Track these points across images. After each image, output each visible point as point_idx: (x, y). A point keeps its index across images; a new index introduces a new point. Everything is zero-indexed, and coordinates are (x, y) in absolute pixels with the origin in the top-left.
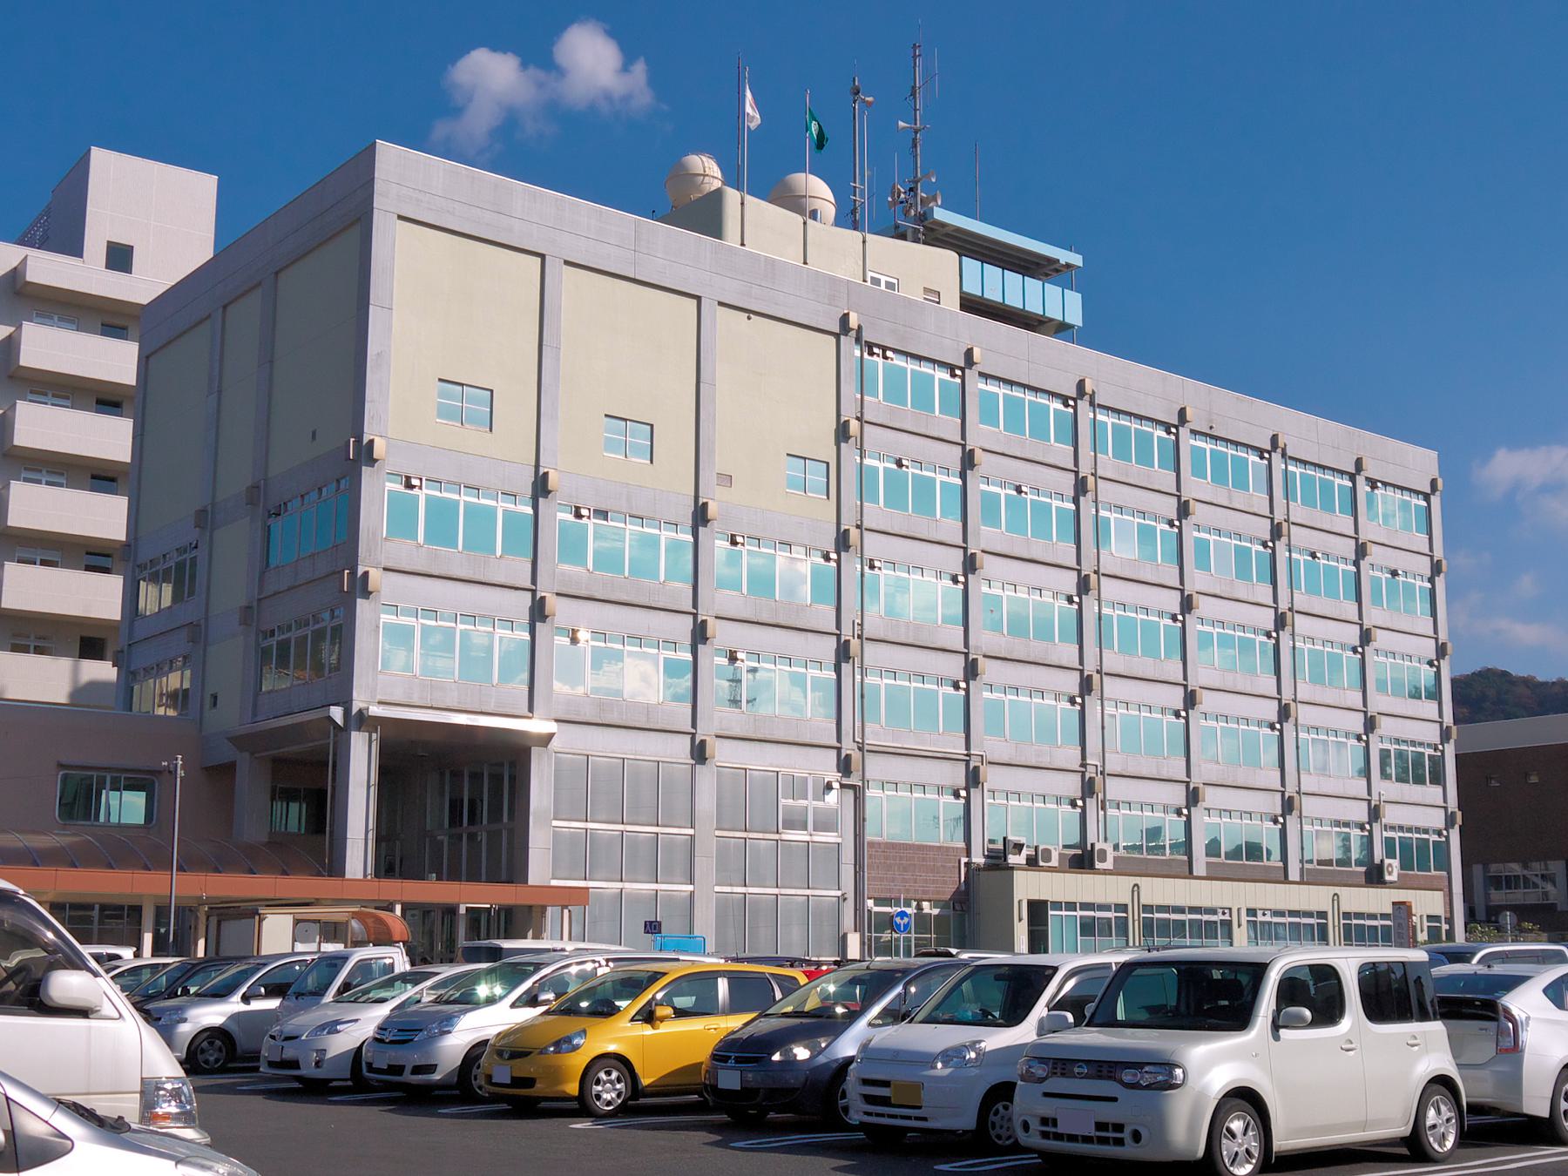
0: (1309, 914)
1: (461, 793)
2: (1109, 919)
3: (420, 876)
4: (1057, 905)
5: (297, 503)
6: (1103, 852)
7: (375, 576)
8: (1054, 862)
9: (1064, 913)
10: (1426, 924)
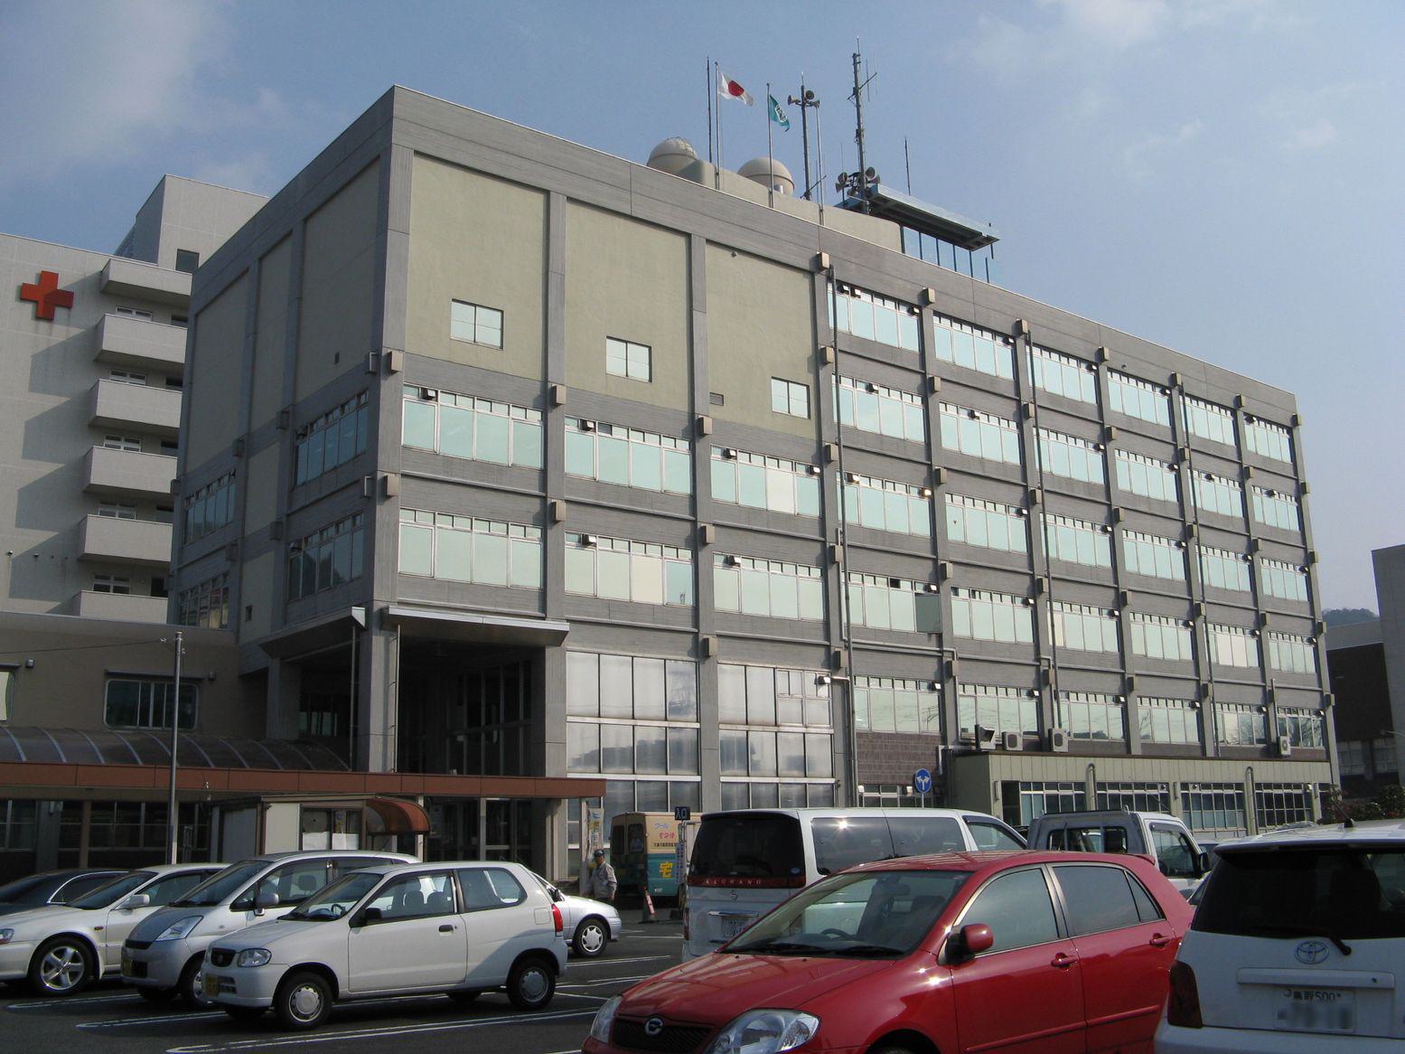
0: (1229, 786)
1: (484, 684)
2: (1071, 796)
3: (442, 770)
4: (1027, 786)
5: (322, 422)
6: (1059, 738)
7: (394, 483)
8: (1019, 747)
9: (1032, 792)
10: (1319, 791)
